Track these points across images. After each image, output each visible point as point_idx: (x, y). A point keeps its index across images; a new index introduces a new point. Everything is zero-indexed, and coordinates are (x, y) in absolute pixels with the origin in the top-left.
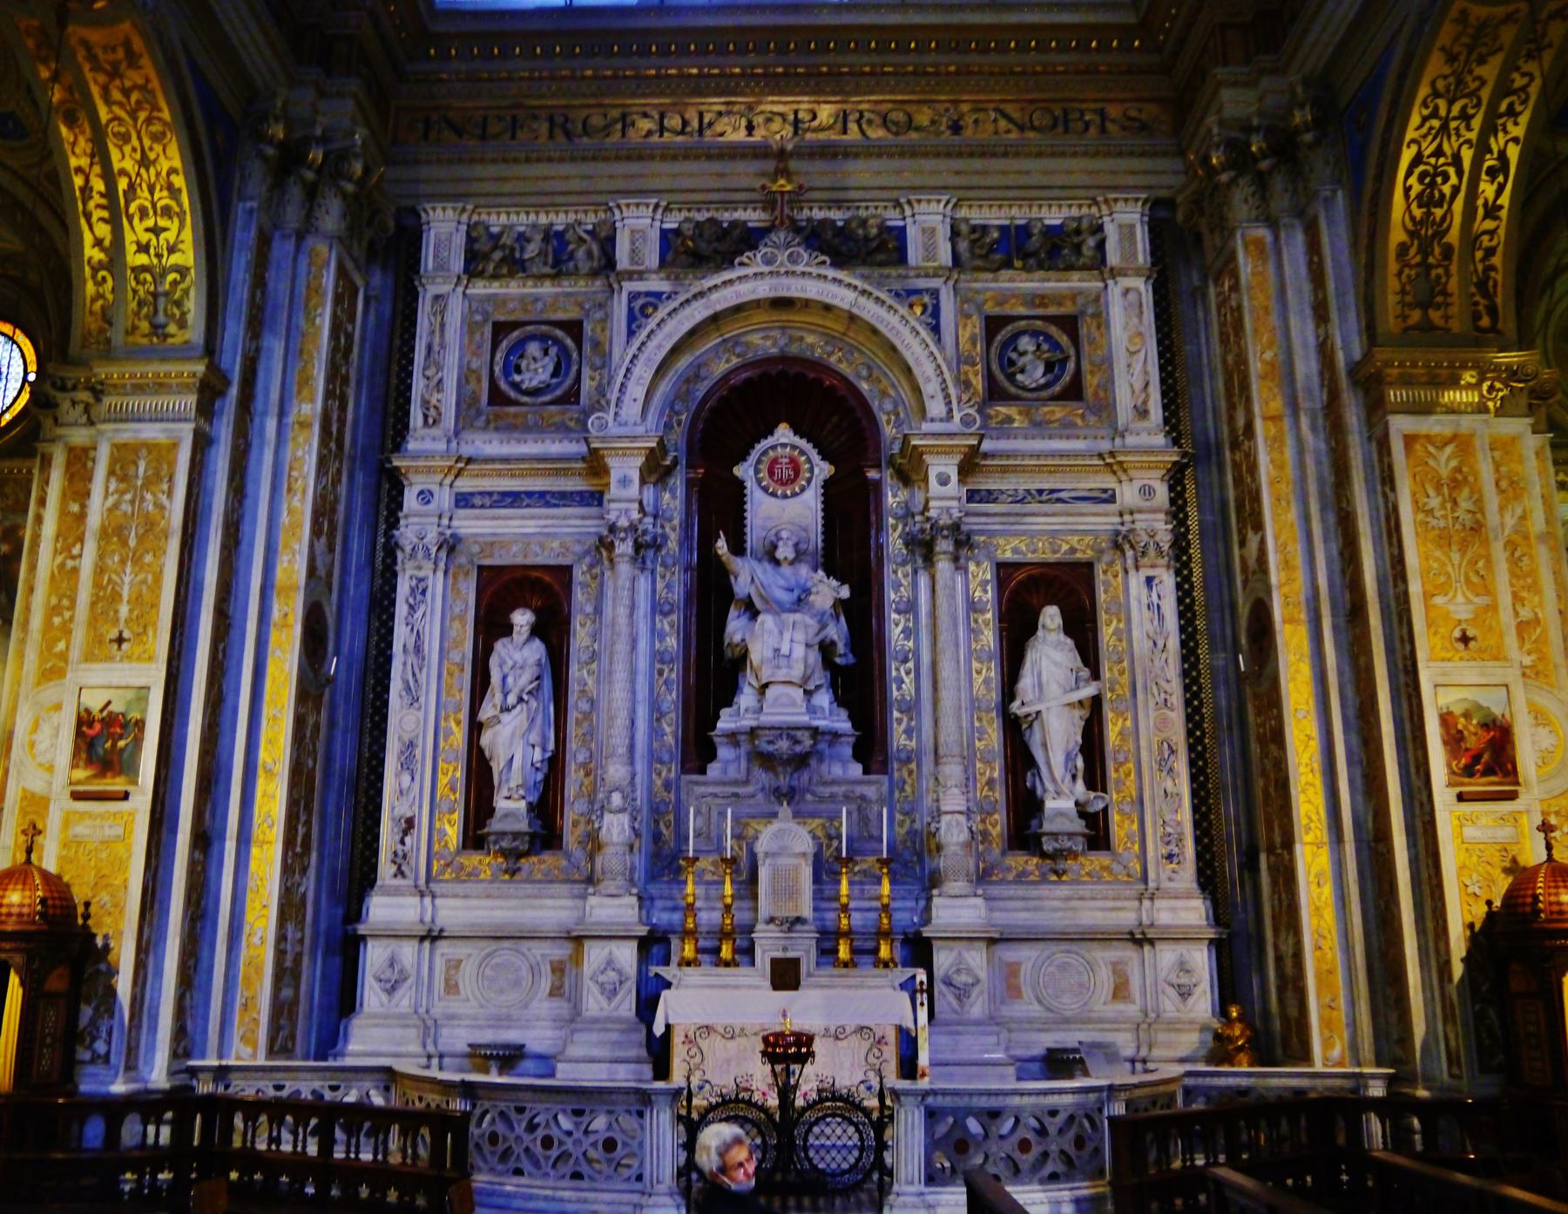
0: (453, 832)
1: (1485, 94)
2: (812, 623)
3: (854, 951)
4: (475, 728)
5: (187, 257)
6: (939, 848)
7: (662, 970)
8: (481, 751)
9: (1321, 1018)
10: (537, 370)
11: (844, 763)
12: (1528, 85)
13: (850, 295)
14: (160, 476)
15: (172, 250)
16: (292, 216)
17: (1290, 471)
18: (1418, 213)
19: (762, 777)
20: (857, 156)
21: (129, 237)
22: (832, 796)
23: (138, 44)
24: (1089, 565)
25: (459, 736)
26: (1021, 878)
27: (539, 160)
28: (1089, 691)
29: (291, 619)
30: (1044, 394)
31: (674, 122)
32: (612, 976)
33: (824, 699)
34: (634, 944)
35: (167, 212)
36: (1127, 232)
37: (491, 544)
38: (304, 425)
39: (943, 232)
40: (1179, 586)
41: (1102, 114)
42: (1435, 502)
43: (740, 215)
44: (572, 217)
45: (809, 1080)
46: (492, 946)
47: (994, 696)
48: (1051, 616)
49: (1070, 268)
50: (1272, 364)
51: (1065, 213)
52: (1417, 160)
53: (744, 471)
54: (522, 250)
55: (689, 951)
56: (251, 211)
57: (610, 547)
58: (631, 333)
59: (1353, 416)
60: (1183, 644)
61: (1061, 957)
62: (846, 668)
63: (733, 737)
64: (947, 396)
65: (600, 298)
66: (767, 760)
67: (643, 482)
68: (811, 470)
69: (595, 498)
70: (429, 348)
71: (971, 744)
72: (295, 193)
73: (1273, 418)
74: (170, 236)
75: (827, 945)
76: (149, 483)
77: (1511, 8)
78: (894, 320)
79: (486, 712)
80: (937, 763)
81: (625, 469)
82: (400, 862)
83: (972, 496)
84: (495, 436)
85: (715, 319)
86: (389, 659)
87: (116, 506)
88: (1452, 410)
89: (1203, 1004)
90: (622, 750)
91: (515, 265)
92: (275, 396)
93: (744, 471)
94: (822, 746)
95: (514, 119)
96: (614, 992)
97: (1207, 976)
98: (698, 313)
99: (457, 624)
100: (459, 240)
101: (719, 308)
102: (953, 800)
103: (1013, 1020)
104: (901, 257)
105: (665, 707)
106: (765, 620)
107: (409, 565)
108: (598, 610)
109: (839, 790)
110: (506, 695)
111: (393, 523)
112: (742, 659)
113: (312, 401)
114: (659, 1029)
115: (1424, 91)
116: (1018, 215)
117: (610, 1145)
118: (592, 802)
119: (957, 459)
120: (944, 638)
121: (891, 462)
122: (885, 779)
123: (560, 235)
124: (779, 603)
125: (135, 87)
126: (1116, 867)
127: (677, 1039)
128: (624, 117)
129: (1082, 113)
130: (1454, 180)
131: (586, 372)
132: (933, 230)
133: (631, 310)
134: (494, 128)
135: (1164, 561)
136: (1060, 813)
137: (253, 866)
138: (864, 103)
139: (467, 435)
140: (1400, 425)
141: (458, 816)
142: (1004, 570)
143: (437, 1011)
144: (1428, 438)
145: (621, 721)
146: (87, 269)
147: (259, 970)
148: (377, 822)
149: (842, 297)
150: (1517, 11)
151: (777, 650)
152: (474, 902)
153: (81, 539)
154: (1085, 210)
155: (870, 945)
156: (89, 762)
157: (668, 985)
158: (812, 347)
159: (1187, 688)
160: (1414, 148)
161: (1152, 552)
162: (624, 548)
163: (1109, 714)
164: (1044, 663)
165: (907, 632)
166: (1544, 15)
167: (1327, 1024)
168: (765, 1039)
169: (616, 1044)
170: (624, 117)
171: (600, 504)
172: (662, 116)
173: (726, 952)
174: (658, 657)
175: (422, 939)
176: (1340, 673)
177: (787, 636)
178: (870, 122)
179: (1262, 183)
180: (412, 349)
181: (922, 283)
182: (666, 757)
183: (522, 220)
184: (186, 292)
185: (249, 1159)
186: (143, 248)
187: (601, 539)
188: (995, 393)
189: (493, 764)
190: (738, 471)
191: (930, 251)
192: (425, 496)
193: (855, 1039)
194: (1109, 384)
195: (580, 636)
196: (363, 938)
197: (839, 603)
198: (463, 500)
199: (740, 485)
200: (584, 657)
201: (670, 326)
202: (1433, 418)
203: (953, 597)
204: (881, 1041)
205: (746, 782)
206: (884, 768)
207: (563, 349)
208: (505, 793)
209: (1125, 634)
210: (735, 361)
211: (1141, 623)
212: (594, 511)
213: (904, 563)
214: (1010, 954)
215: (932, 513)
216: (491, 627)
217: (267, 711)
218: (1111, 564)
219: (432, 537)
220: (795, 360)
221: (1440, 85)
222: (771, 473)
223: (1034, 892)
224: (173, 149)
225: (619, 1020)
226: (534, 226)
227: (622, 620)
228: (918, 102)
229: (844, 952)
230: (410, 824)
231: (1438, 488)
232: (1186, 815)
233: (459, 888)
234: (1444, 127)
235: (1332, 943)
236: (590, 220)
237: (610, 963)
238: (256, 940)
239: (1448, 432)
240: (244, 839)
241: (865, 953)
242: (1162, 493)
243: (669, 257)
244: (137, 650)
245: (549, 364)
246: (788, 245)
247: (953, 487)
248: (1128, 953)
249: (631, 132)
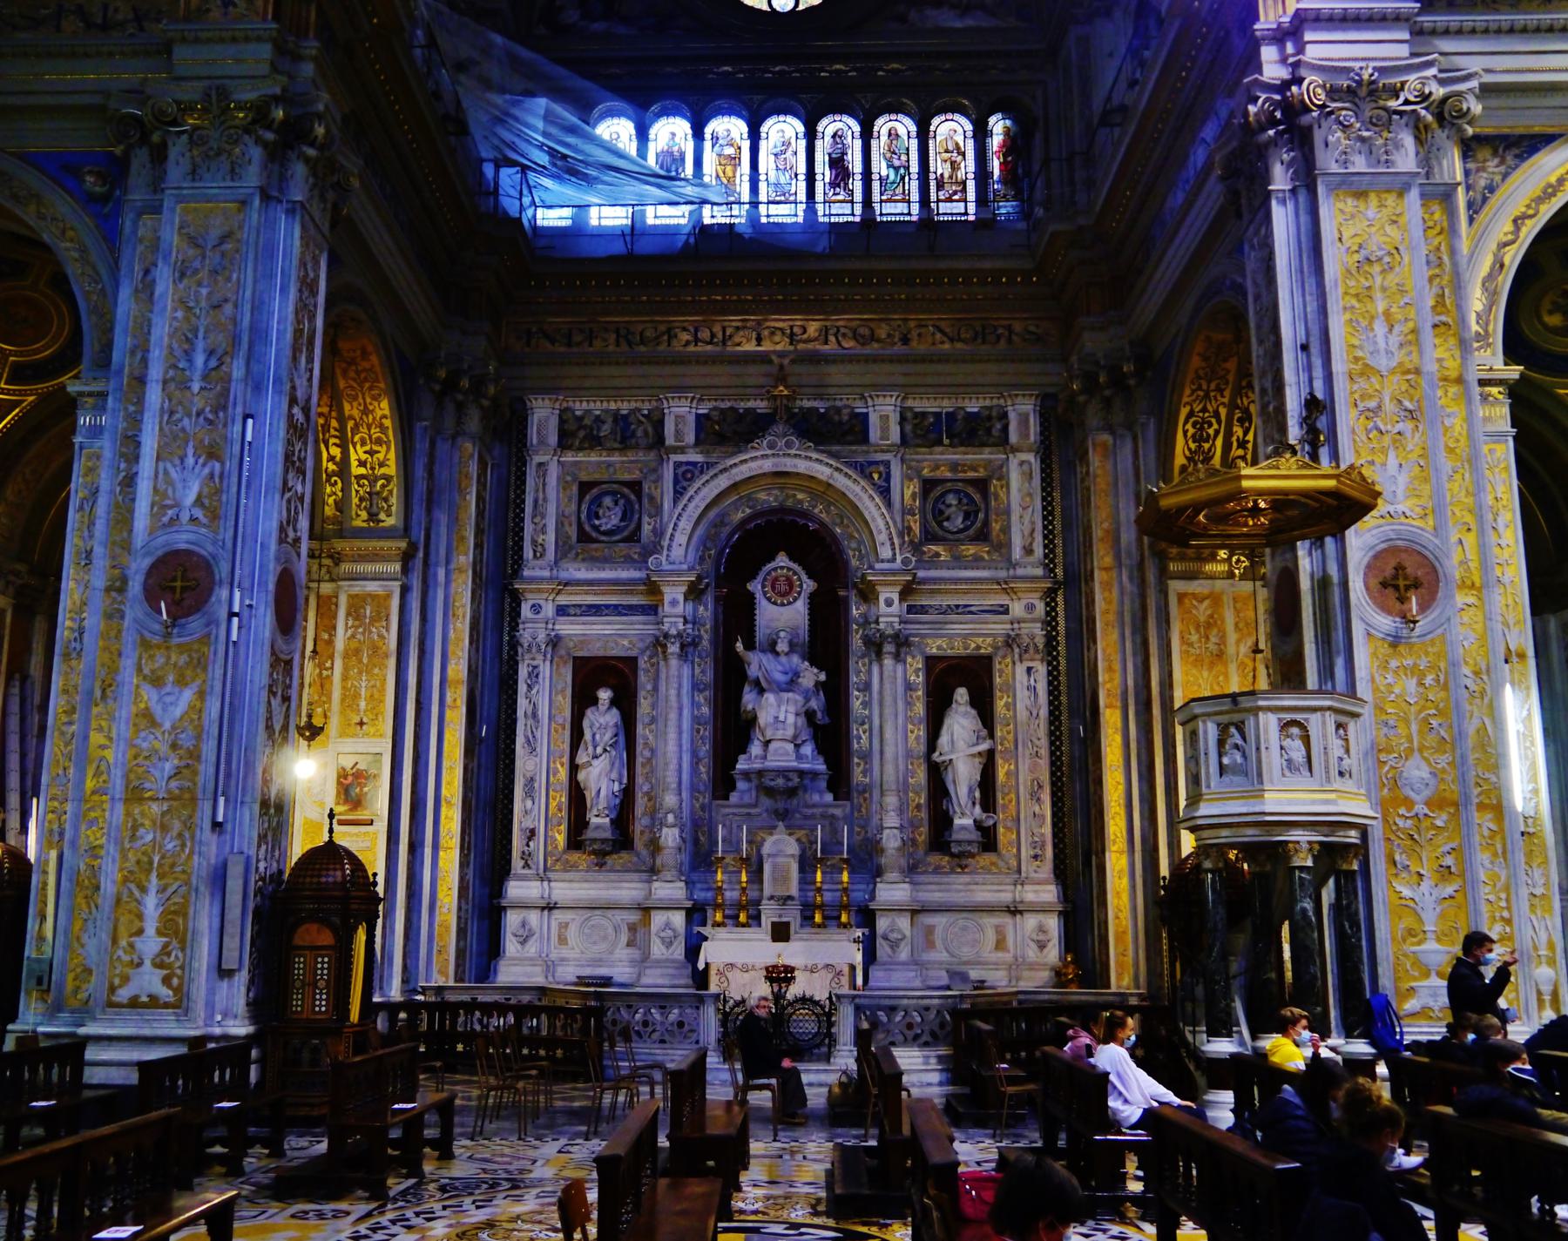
0: (561, 839)
1: (1231, 378)
2: (799, 698)
3: (825, 917)
4: (574, 768)
5: (391, 469)
6: (883, 850)
7: (701, 929)
8: (578, 783)
9: (1117, 962)
10: (611, 518)
11: (821, 792)
13: (828, 471)
14: (381, 615)
15: (381, 465)
16: (449, 423)
17: (1114, 607)
18: (1193, 446)
19: (766, 802)
20: (834, 362)
21: (353, 456)
22: (813, 816)
23: (370, 348)
24: (988, 659)
25: (563, 774)
26: (937, 870)
27: (610, 364)
28: (984, 746)
29: (459, 702)
30: (961, 536)
31: (705, 334)
32: (670, 933)
33: (808, 749)
34: (683, 913)
35: (379, 442)
36: (1024, 420)
37: (585, 640)
38: (460, 570)
39: (894, 419)
40: (1050, 673)
41: (1009, 328)
42: (1194, 638)
43: (751, 404)
44: (633, 405)
45: (793, 991)
46: (588, 913)
47: (923, 748)
48: (961, 694)
49: (983, 445)
50: (1107, 531)
51: (981, 403)
52: (1191, 414)
53: (755, 586)
54: (599, 429)
55: (719, 917)
56: (426, 428)
57: (664, 647)
58: (675, 501)
59: (1151, 577)
60: (1051, 713)
61: (961, 922)
62: (824, 726)
63: (746, 775)
64: (893, 544)
65: (653, 465)
66: (770, 792)
67: (686, 599)
68: (801, 586)
69: (652, 610)
70: (536, 501)
71: (906, 783)
72: (450, 407)
73: (1106, 569)
74: (381, 456)
75: (808, 914)
76: (372, 620)
78: (857, 489)
79: (582, 758)
80: (882, 795)
81: (674, 593)
82: (526, 857)
83: (911, 610)
84: (583, 566)
85: (734, 487)
86: (515, 721)
87: (353, 636)
88: (1212, 577)
89: (1053, 954)
90: (674, 786)
91: (593, 441)
92: (442, 552)
93: (755, 586)
94: (806, 782)
95: (591, 331)
96: (671, 943)
97: (1056, 934)
98: (723, 482)
99: (560, 698)
100: (554, 423)
101: (738, 479)
102: (892, 820)
103: (929, 962)
104: (864, 439)
105: (702, 754)
106: (770, 697)
107: (527, 656)
108: (656, 689)
109: (817, 811)
110: (595, 747)
111: (514, 627)
112: (752, 721)
113: (466, 554)
114: (701, 966)
115: (1191, 375)
116: (946, 405)
117: (681, 1024)
118: (653, 819)
119: (898, 589)
120: (888, 711)
121: (855, 585)
122: (848, 803)
123: (625, 417)
124: (778, 684)
125: (365, 370)
126: (1001, 864)
127: (713, 972)
128: (669, 330)
129: (996, 328)
130: (1216, 426)
131: (646, 519)
132: (887, 417)
133: (676, 475)
134: (577, 338)
135: (1039, 656)
136: (963, 828)
137: (441, 863)
138: (841, 320)
139: (564, 564)
140: (1176, 586)
141: (564, 828)
142: (931, 661)
143: (553, 956)
144: (1194, 596)
145: (673, 766)
147: (447, 929)
148: (510, 832)
149: (822, 471)
151: (776, 717)
152: (575, 885)
153: (332, 657)
154: (995, 402)
155: (835, 914)
156: (346, 801)
157: (706, 939)
158: (800, 502)
159: (1052, 743)
160: (1188, 409)
161: (1031, 650)
162: (674, 648)
163: (999, 761)
164: (956, 727)
165: (865, 704)
167: (1120, 965)
168: (767, 969)
169: (673, 976)
170: (669, 330)
171: (656, 613)
172: (696, 330)
173: (743, 918)
174: (696, 720)
175: (543, 909)
176: (1138, 742)
177: (783, 708)
178: (844, 335)
179: (1107, 403)
180: (523, 501)
181: (880, 457)
182: (702, 788)
183: (598, 407)
184: (391, 492)
185: (468, 1037)
186: (362, 464)
187: (657, 639)
188: (929, 537)
189: (587, 793)
190: (750, 587)
191: (885, 430)
192: (536, 609)
193: (823, 972)
194: (1006, 530)
195: (644, 707)
196: (505, 908)
197: (818, 684)
198: (562, 611)
199: (752, 596)
200: (647, 720)
201: (705, 491)
202: (1196, 582)
203: (894, 682)
204: (840, 973)
205: (755, 806)
206: (848, 797)
207: (628, 501)
208: (595, 812)
209: (1011, 706)
210: (748, 511)
211: (1023, 696)
212: (651, 618)
213: (863, 657)
214: (929, 920)
215: (882, 626)
216: (583, 700)
217: (446, 764)
218: (1004, 657)
219: (542, 637)
220: (791, 511)
221: (1201, 373)
222: (773, 588)
223: (945, 879)
224: (385, 404)
225: (673, 961)
226: (607, 411)
227: (673, 698)
228: (881, 320)
229: (818, 918)
230: (532, 833)
231: (1198, 627)
232: (1047, 830)
233: (568, 876)
234: (1207, 396)
235: (1126, 914)
236: (646, 407)
237: (668, 925)
238: (445, 910)
239: (1206, 591)
240: (436, 847)
241: (831, 919)
242: (1040, 608)
243: (702, 436)
244: (372, 730)
245: (618, 511)
246: (785, 435)
247: (895, 608)
248: (1007, 920)
249: (674, 342)
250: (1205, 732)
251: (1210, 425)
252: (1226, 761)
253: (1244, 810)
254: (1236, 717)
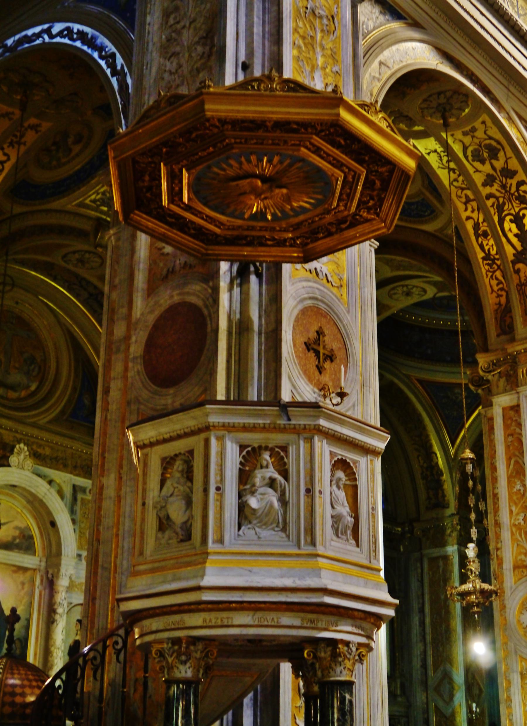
12: (5, 162)
77: (10, 110)
146: (46, 26)
150: (13, 113)
166: (26, 124)
250: (222, 454)
252: (253, 502)
253: (288, 582)
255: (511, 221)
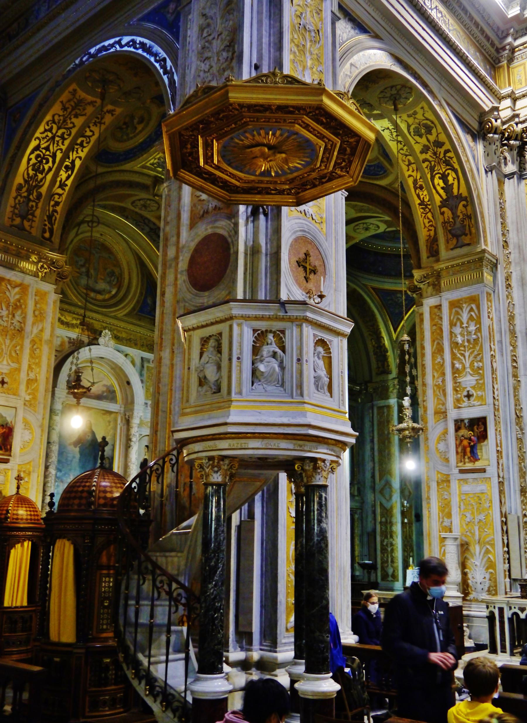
1: (74, 131)
18: (31, 172)
34: (486, 620)
52: (37, 148)
130: (50, 164)
160: (37, 142)
234: (53, 138)
239: (18, 281)
250: (241, 335)
251: (47, 162)
252: (262, 367)
254: (277, 325)
255: (440, 178)
